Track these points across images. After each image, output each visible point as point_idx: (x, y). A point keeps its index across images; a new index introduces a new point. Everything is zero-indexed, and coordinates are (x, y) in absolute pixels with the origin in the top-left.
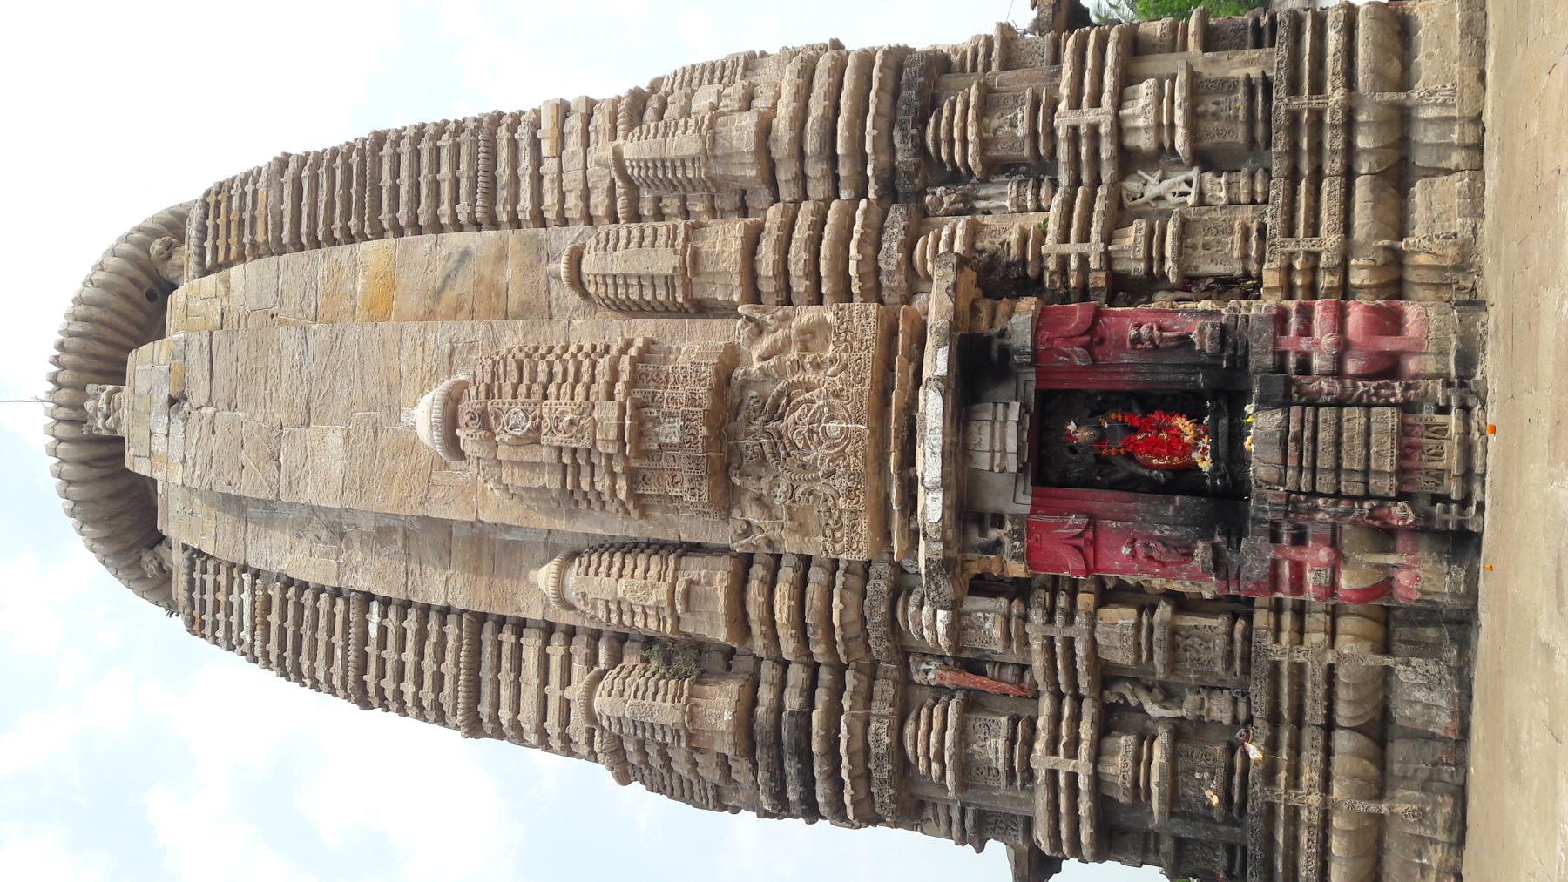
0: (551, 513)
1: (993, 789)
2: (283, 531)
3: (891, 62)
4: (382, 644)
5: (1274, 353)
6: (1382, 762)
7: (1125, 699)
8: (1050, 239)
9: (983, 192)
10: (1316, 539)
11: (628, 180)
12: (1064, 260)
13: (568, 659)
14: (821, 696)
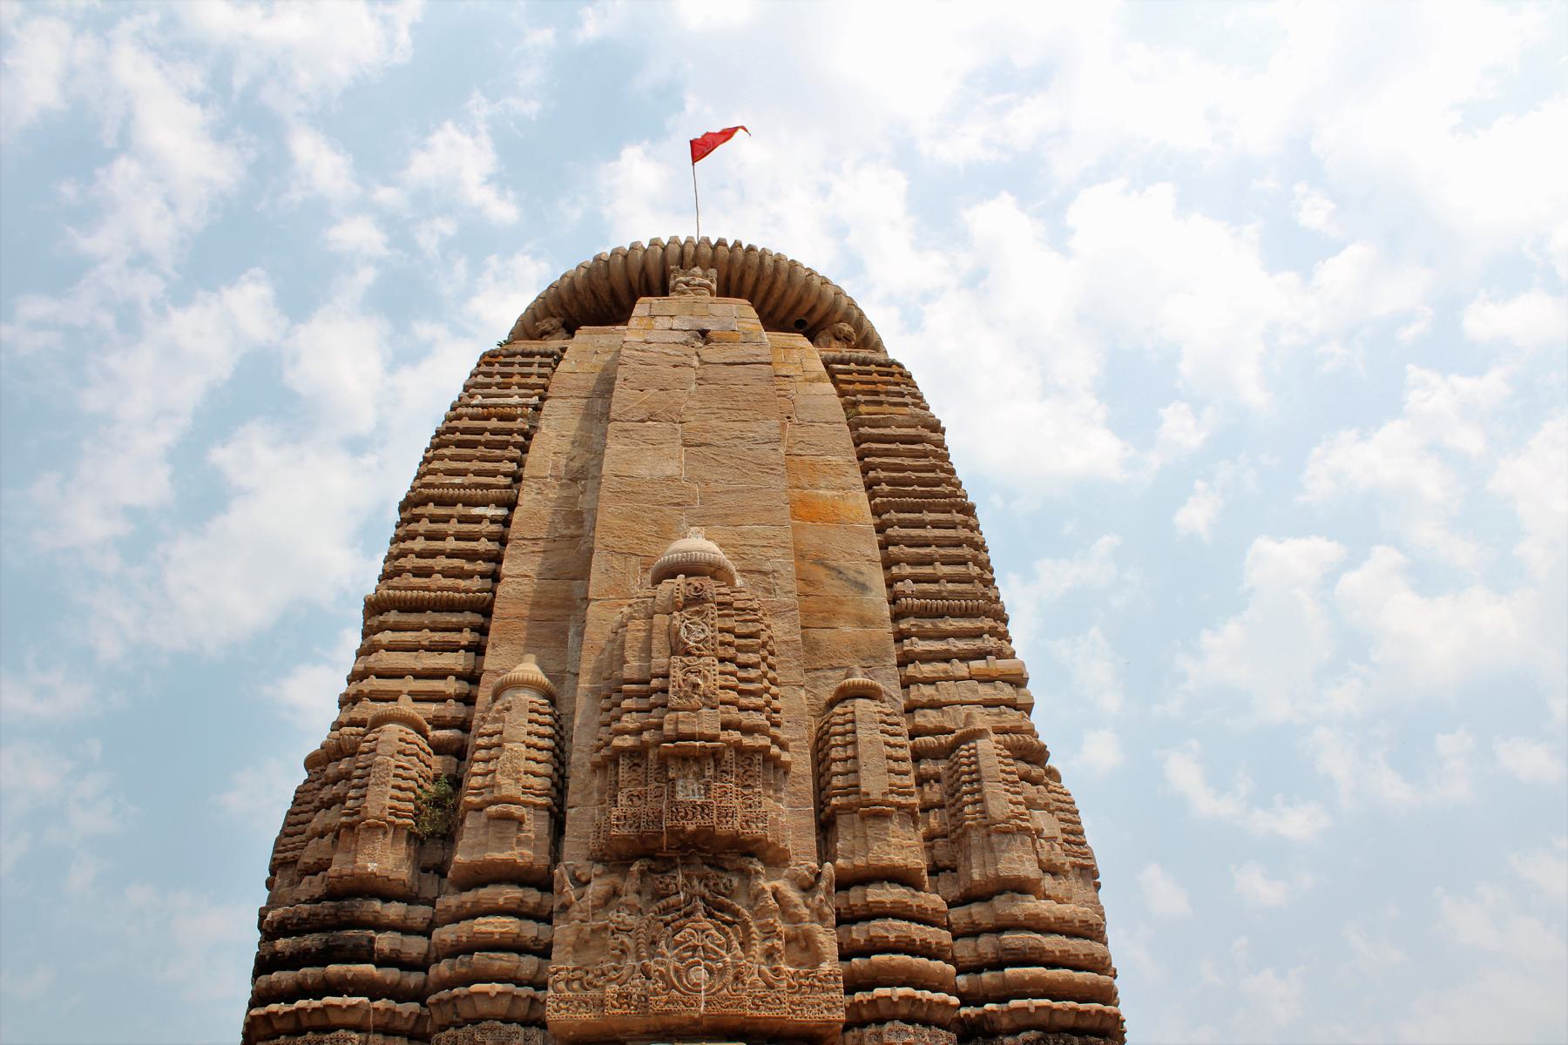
0: (597, 671)
2: (580, 429)
3: (1109, 1023)
4: (463, 519)
11: (954, 746)
13: (440, 698)
14: (391, 974)
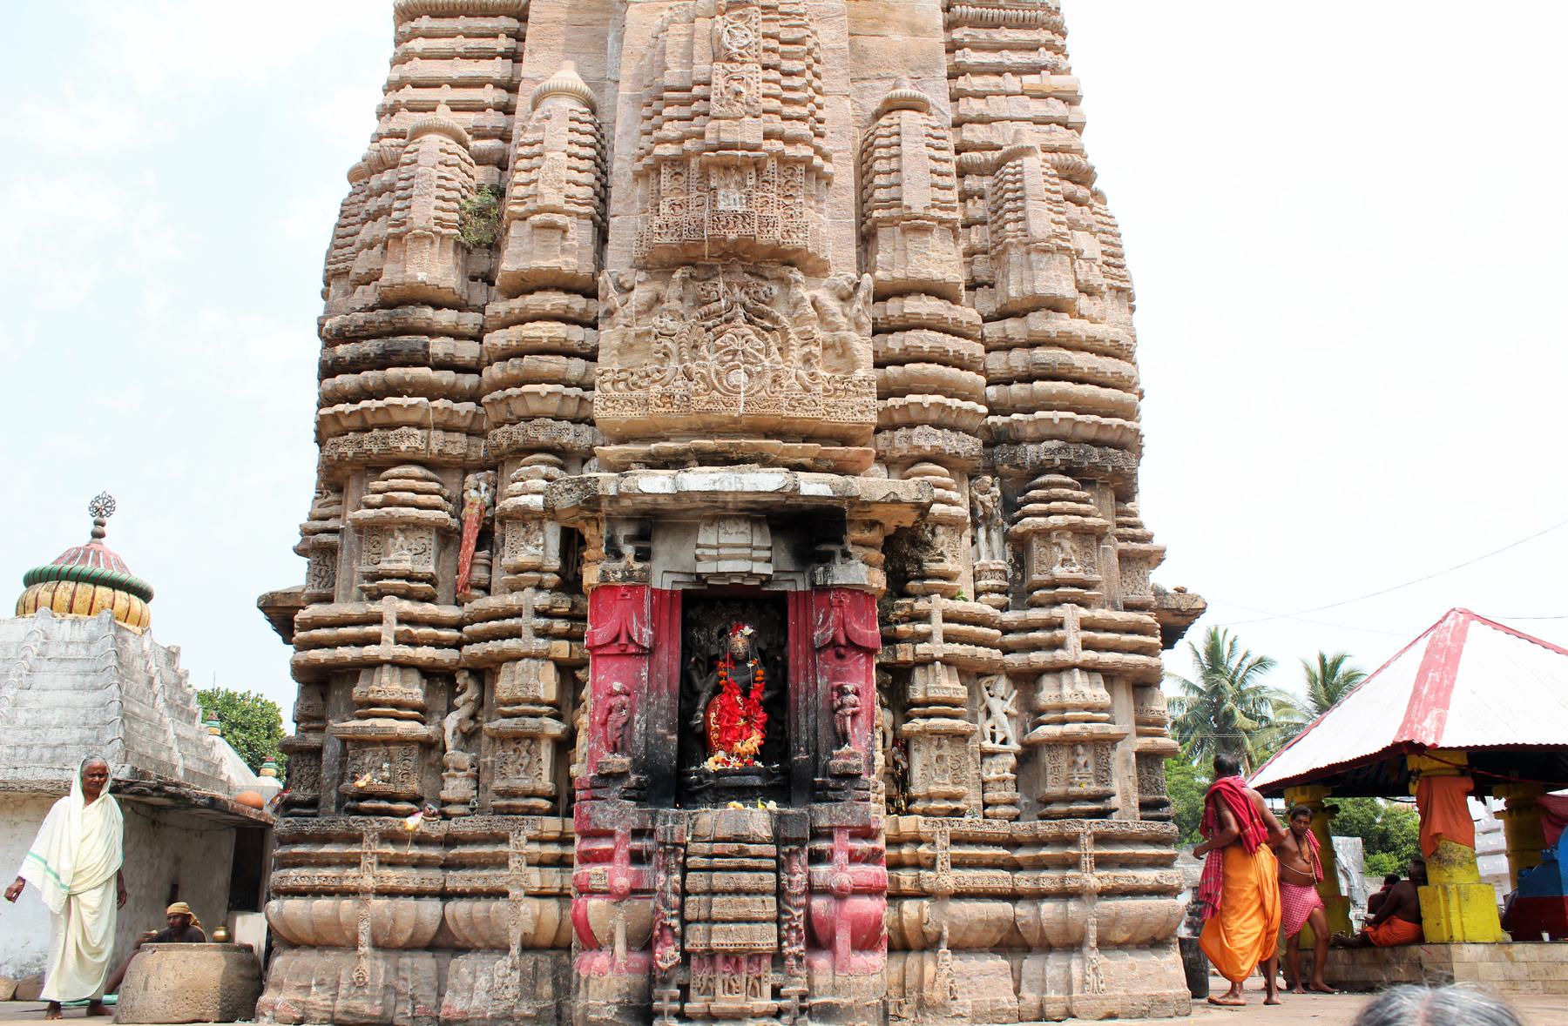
0: (638, 78)
1: (359, 561)
3: (1128, 438)
5: (831, 827)
6: (412, 947)
7: (460, 693)
8: (946, 603)
9: (995, 535)
10: (638, 873)
11: (1000, 164)
12: (925, 618)
14: (447, 377)
